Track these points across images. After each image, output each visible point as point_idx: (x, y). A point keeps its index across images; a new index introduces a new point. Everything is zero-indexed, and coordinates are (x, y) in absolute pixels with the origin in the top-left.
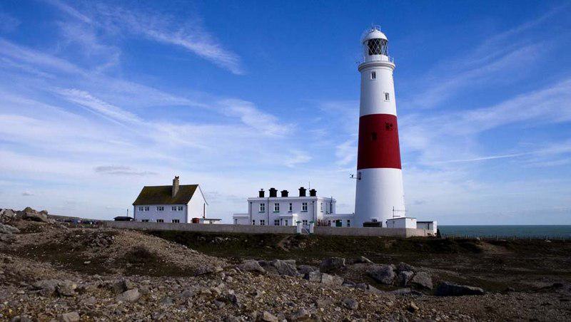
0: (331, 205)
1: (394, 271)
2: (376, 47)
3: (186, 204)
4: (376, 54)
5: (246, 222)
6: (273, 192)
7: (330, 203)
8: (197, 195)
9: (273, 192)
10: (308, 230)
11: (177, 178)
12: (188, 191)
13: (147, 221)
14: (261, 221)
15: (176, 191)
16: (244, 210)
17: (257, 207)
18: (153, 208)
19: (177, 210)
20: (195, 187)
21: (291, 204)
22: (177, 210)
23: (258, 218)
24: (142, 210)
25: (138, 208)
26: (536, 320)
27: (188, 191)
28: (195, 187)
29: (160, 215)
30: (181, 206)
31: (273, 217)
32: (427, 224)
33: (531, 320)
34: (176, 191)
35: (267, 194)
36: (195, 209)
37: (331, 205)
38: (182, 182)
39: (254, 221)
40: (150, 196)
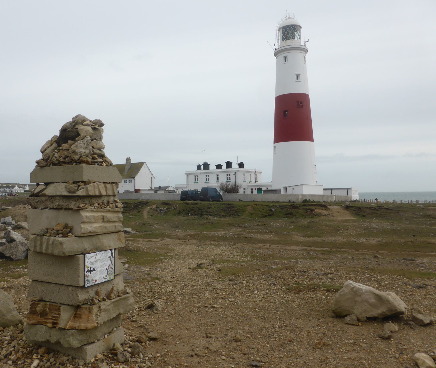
0: (256, 175)
3: (134, 178)
4: (289, 39)
6: (229, 165)
15: (127, 168)
16: (25, 179)
21: (244, 175)
24: (127, 182)
28: (142, 164)
32: (346, 191)
34: (127, 168)
35: (224, 166)
36: (142, 182)
37: (256, 175)
38: (132, 161)
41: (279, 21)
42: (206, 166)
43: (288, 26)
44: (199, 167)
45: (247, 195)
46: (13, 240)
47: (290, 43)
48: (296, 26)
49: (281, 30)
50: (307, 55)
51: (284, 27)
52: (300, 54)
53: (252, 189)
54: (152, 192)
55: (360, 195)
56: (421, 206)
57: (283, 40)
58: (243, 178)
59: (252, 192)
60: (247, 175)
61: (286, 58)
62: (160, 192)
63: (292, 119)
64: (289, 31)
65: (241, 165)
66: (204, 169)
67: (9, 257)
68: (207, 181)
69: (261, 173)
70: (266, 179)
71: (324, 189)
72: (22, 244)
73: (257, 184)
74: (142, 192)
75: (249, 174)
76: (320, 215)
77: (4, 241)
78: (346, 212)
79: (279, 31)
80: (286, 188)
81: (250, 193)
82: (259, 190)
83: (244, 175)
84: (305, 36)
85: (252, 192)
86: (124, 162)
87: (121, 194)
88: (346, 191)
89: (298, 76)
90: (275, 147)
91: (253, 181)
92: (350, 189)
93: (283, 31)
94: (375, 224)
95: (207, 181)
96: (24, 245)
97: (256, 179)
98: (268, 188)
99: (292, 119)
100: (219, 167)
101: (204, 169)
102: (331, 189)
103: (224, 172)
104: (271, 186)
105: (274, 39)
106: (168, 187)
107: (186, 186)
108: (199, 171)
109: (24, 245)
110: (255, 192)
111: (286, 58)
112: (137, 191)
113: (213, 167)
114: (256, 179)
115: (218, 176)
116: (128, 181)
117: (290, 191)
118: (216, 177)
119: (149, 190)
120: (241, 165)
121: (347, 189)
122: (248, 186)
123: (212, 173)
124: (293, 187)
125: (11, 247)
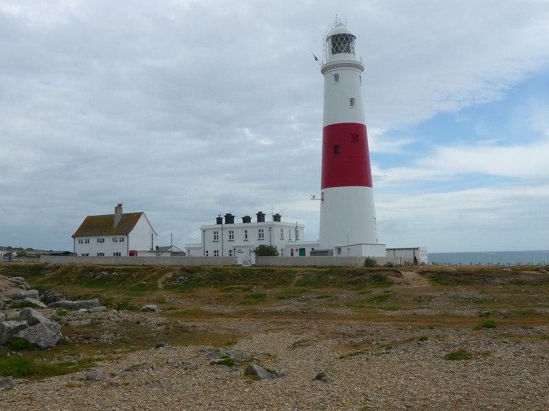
0: (296, 232)
1: (95, 324)
2: (339, 44)
3: (127, 235)
4: (340, 52)
5: (200, 254)
6: (261, 217)
7: (297, 229)
8: (141, 221)
9: (261, 217)
10: (250, 261)
11: (120, 205)
12: (130, 220)
13: (87, 255)
14: (215, 252)
15: (117, 221)
16: (195, 237)
17: (210, 235)
18: (93, 240)
19: (84, 243)
20: (138, 215)
21: (282, 230)
22: (84, 243)
23: (211, 247)
24: (116, 241)
25: (77, 240)
26: (378, 409)
27: (130, 220)
28: (138, 215)
29: (101, 248)
30: (81, 238)
31: (229, 246)
32: (412, 251)
33: (125, 409)
34: (117, 221)
35: (254, 219)
36: (139, 240)
37: (296, 232)
38: (125, 211)
39: (207, 252)
40: (94, 227)
41: (327, 29)
42: (230, 219)
43: (339, 35)
44: (219, 221)
45: (286, 258)
46: (36, 322)
47: (342, 57)
48: (350, 35)
49: (330, 40)
50: (363, 74)
51: (333, 37)
52: (357, 73)
53: (292, 250)
54: (154, 255)
55: (430, 256)
56: (509, 270)
57: (333, 53)
58: (280, 235)
59: (292, 254)
60: (286, 231)
61: (337, 77)
62: (164, 255)
63: (345, 156)
64: (341, 42)
65: (277, 218)
66: (227, 223)
67: (36, 345)
68: (262, 238)
69: (303, 228)
70: (312, 234)
71: (387, 250)
72: (49, 326)
73: (298, 243)
74: (139, 255)
75: (244, 230)
76: (391, 283)
77: (25, 322)
78: (422, 278)
79: (327, 40)
80: (339, 249)
81: (228, 255)
82: (302, 251)
83: (282, 230)
84: (360, 51)
85: (292, 254)
86: (112, 212)
87: (210, 258)
88: (412, 251)
89: (352, 101)
90: (323, 193)
91: (293, 238)
92: (417, 249)
93: (332, 40)
94: (464, 292)
95: (262, 238)
96: (52, 327)
97: (297, 236)
98: (313, 249)
99: (345, 156)
100: (246, 219)
101: (227, 223)
102: (394, 250)
103: (256, 227)
104: (318, 245)
105: (322, 50)
106: (171, 247)
107: (201, 246)
108: (220, 226)
109: (52, 327)
110: (296, 254)
111: (337, 77)
112: (132, 253)
113: (238, 221)
114: (297, 236)
115: (246, 232)
116: (84, 241)
117: (344, 253)
118: (244, 234)
119: (149, 252)
120: (277, 218)
121: (414, 249)
122: (287, 246)
123: (238, 228)
124: (348, 247)
125: (35, 331)
